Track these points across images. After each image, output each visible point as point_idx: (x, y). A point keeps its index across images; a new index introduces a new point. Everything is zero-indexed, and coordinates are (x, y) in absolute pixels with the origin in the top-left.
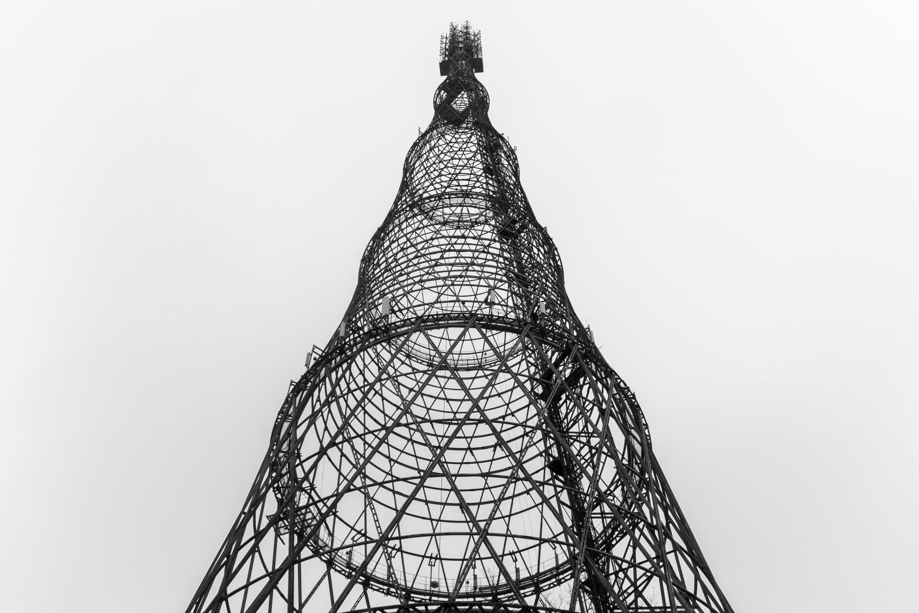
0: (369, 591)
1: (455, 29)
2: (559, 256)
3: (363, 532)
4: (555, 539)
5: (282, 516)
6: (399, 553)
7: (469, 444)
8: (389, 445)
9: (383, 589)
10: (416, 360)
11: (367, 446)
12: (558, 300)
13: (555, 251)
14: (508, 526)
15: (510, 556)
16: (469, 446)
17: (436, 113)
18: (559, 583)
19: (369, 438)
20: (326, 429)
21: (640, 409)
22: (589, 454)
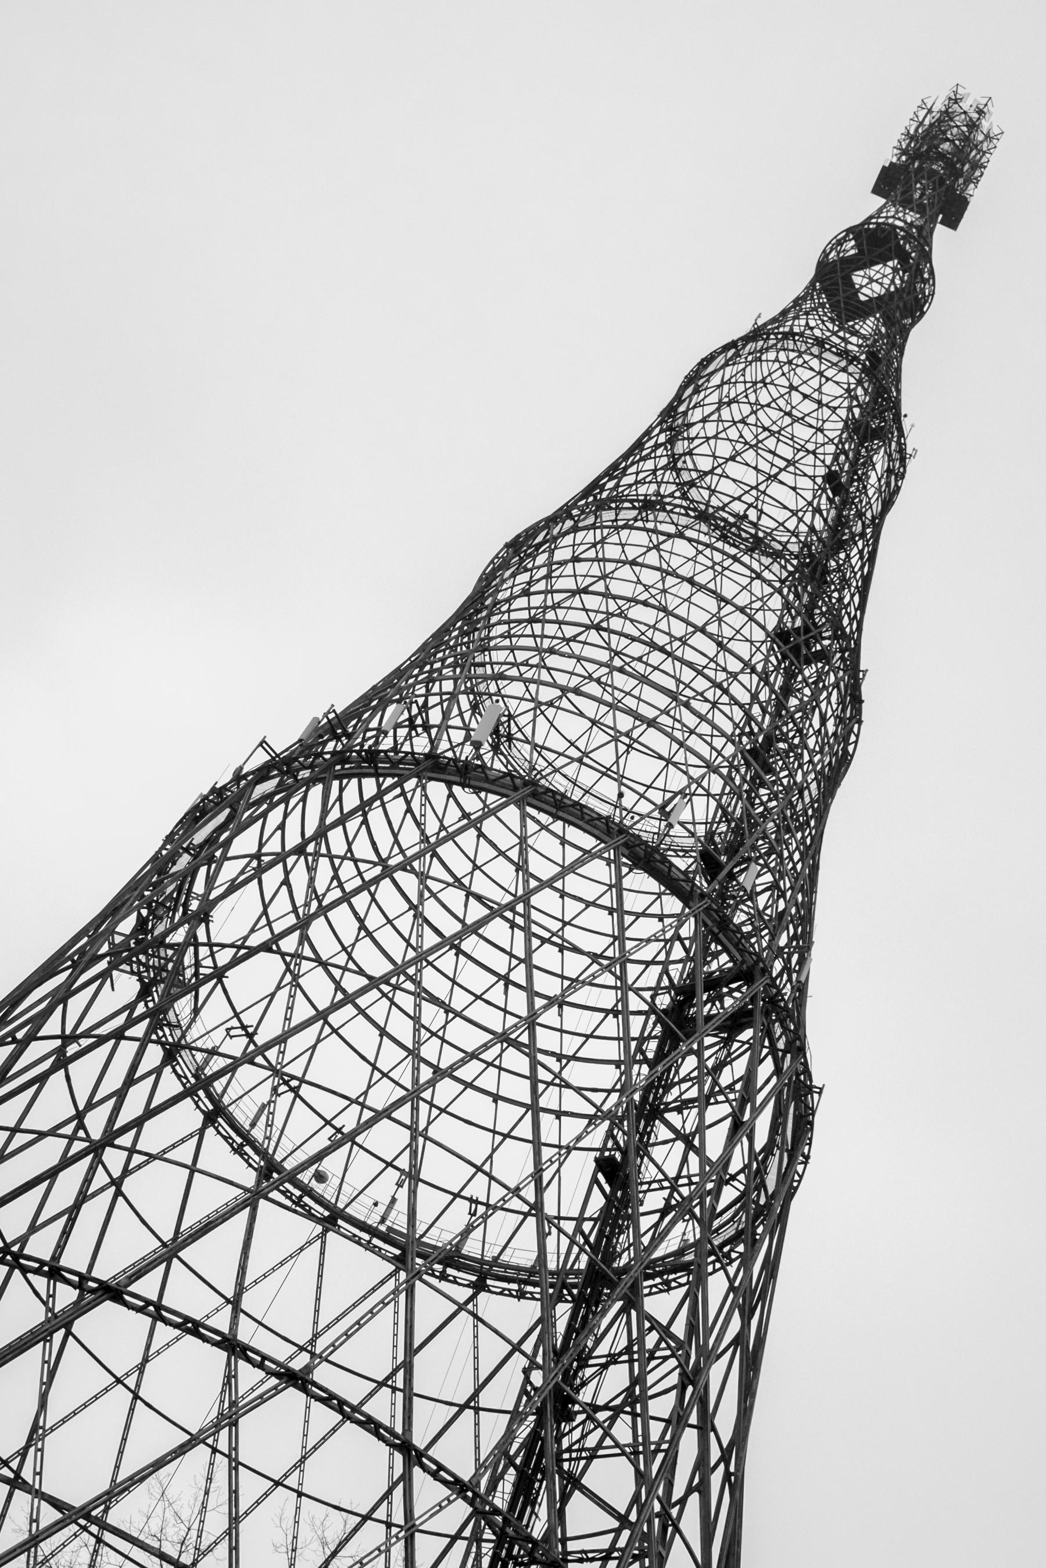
0: (210, 1132)
1: (956, 101)
2: (857, 736)
3: (251, 1030)
4: (556, 1221)
5: (133, 946)
6: (291, 1095)
7: (510, 970)
8: (373, 899)
9: (234, 1141)
10: (505, 761)
11: (335, 884)
12: (812, 806)
13: (856, 726)
14: (494, 1150)
15: (467, 1203)
16: (508, 973)
17: (816, 275)
18: (521, 1295)
19: (347, 870)
20: (282, 827)
21: (812, 1129)
22: (729, 499)
